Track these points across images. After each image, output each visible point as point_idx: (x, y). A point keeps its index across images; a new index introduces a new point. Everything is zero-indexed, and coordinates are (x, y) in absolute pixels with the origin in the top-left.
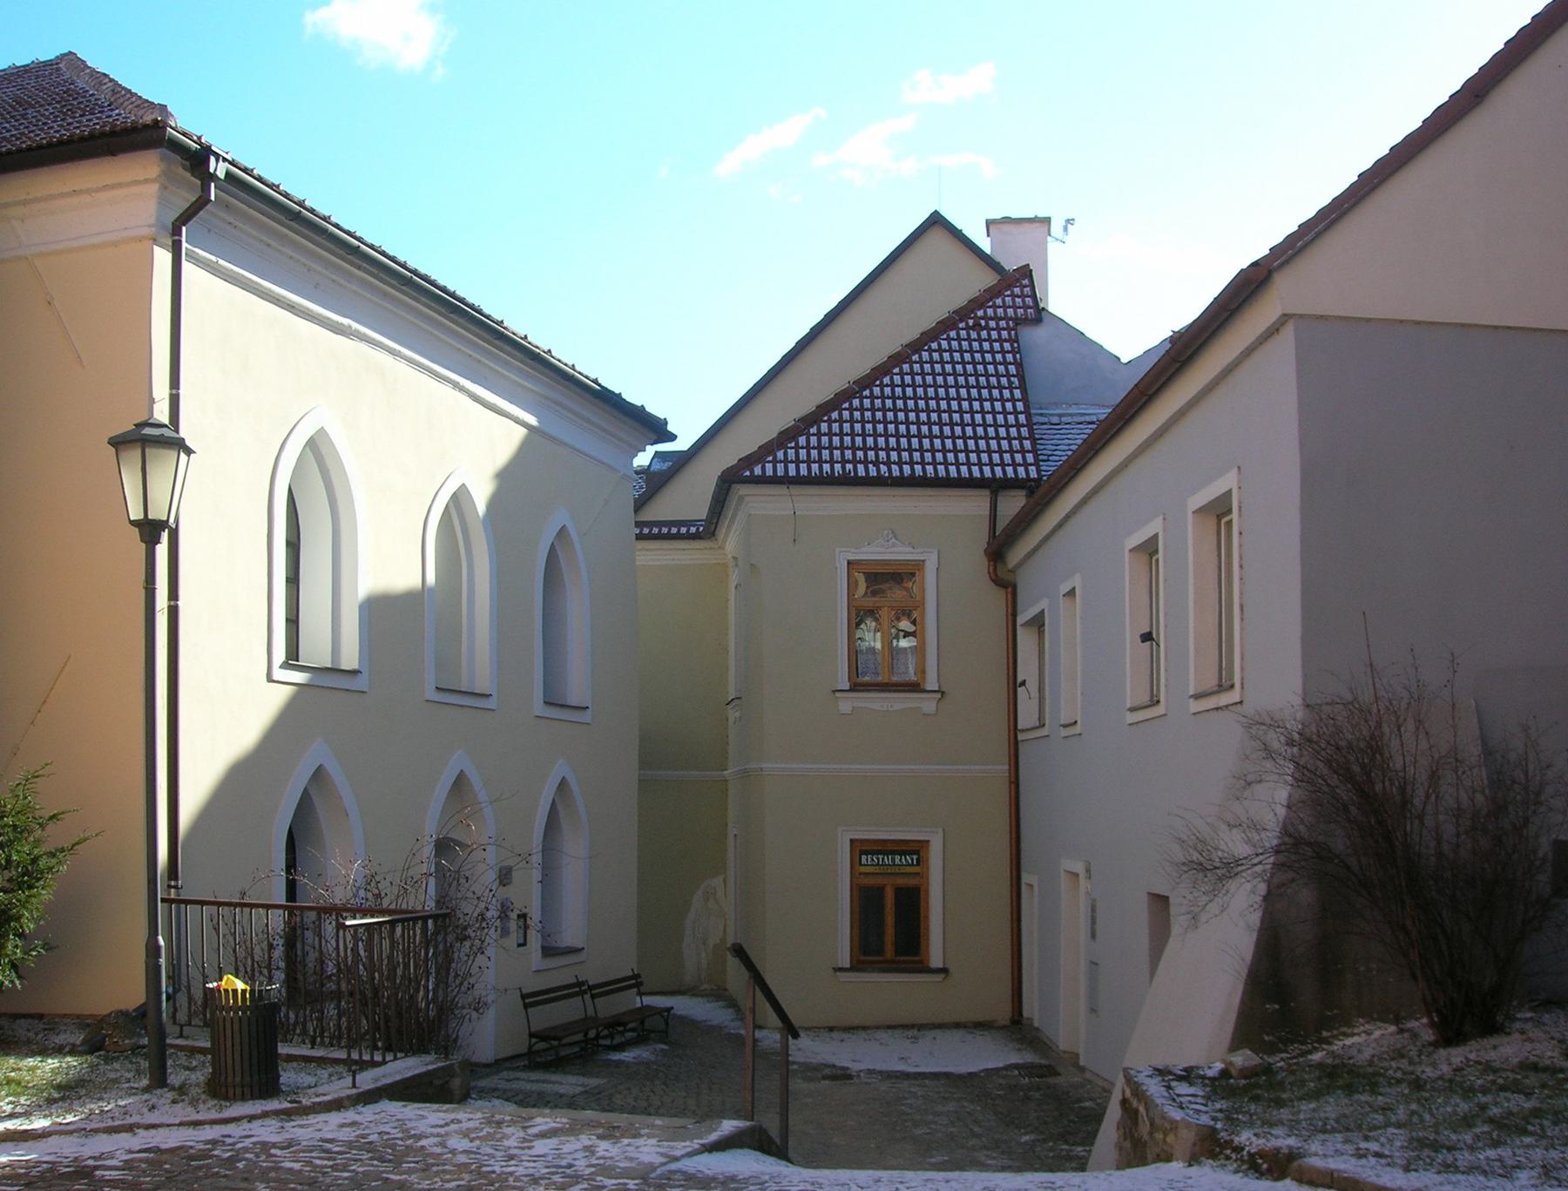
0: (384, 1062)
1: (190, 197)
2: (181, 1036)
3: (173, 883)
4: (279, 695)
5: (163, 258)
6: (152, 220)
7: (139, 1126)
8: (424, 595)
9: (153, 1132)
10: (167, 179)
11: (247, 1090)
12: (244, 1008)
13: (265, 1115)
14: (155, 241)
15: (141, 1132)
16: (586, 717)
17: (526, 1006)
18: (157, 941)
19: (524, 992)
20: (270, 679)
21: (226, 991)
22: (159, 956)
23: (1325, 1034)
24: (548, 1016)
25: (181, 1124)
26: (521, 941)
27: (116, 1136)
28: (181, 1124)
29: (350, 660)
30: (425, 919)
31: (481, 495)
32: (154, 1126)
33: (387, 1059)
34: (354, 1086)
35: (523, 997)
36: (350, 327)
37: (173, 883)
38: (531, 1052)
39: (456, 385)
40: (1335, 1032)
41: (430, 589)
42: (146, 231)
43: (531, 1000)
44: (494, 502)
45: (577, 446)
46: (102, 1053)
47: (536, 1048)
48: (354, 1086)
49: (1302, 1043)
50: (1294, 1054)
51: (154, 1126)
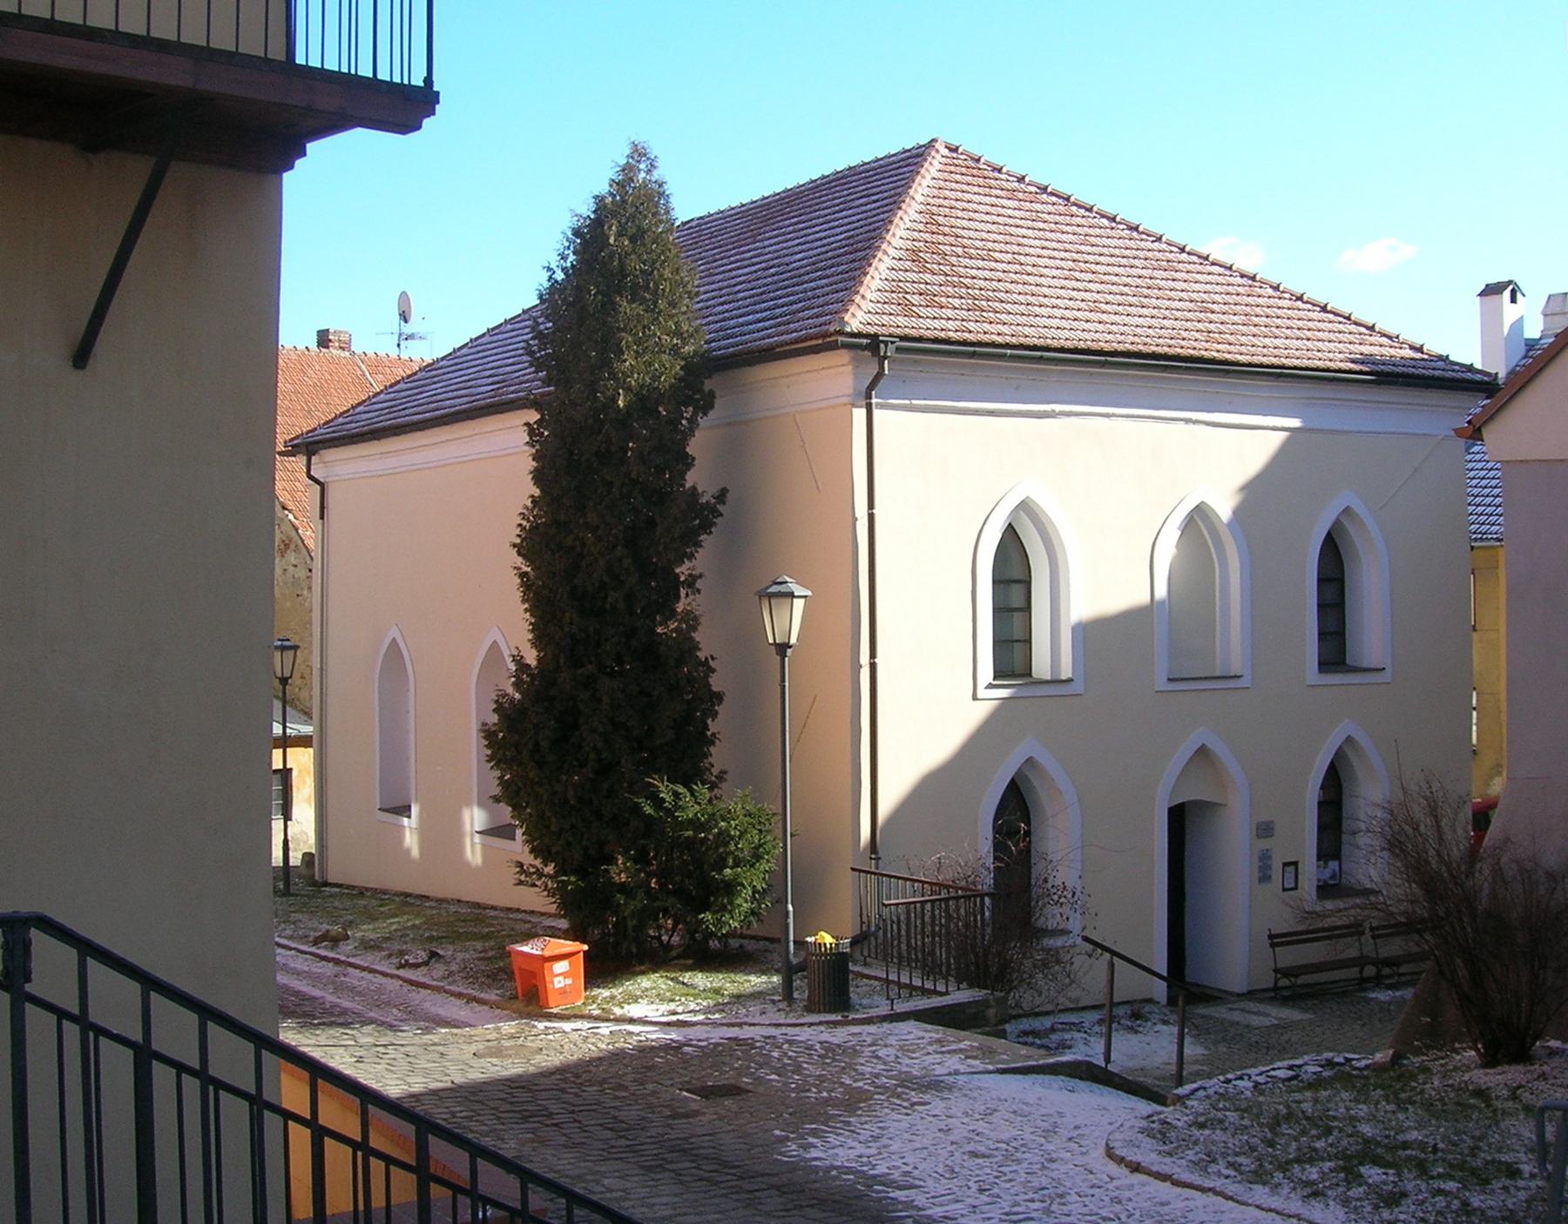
0: (947, 993)
1: (873, 370)
2: (865, 964)
3: (873, 856)
4: (981, 711)
5: (859, 415)
6: (851, 391)
7: (746, 1024)
8: (1152, 610)
9: (752, 1028)
10: (856, 363)
11: (822, 1008)
12: (832, 954)
13: (820, 1023)
14: (854, 405)
15: (746, 1027)
16: (1386, 676)
17: (1273, 945)
18: (786, 907)
19: (1273, 932)
20: (975, 698)
21: (820, 944)
22: (787, 917)
23: (1457, 1045)
24: (1291, 956)
25: (769, 1025)
26: (1290, 884)
27: (732, 1029)
28: (769, 1025)
29: (1066, 672)
30: (982, 896)
31: (1224, 508)
32: (754, 1025)
33: (950, 989)
34: (892, 1009)
35: (1271, 937)
36: (1053, 411)
37: (873, 856)
38: (1276, 988)
39: (1188, 421)
40: (1464, 1045)
41: (1162, 603)
42: (846, 400)
43: (1276, 940)
44: (1238, 512)
45: (1365, 429)
46: (805, 973)
47: (1280, 984)
48: (892, 1009)
49: (1440, 1050)
50: (1432, 1058)
51: (754, 1025)
